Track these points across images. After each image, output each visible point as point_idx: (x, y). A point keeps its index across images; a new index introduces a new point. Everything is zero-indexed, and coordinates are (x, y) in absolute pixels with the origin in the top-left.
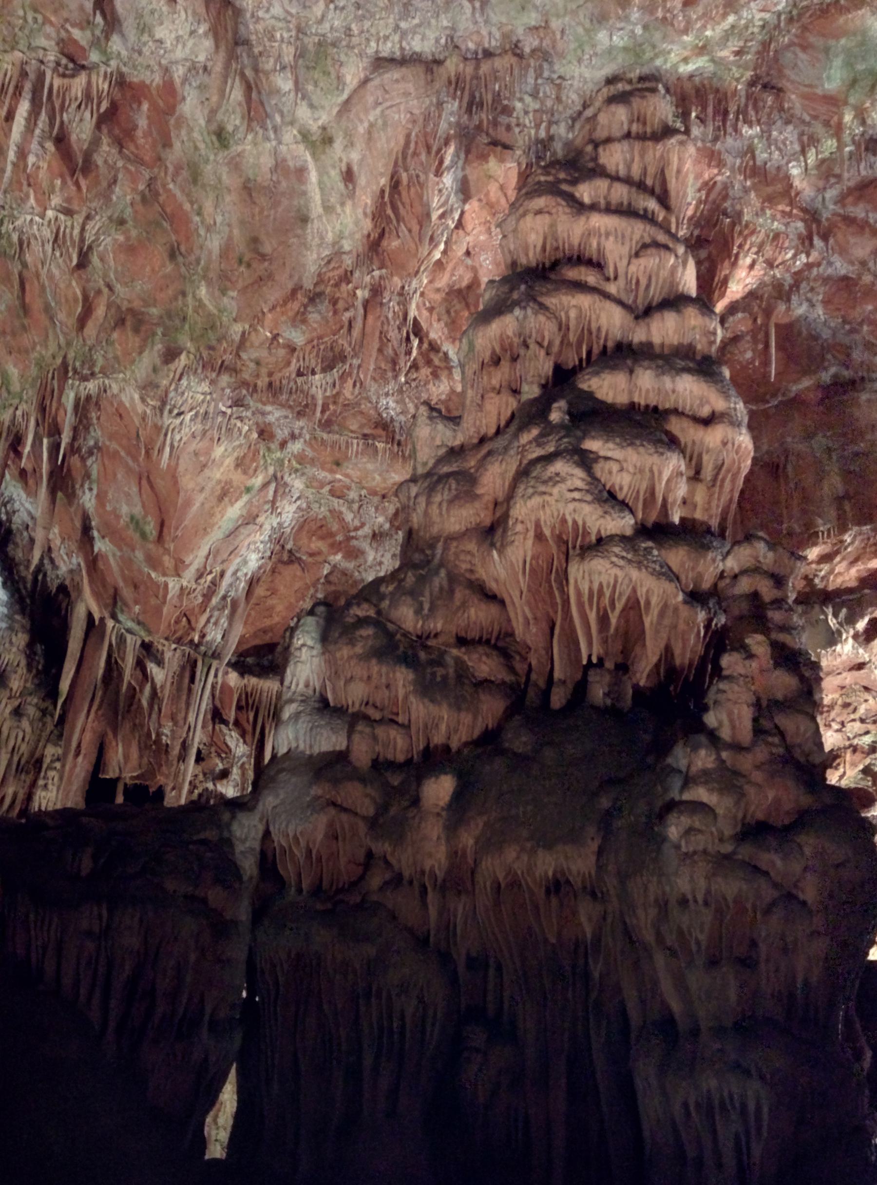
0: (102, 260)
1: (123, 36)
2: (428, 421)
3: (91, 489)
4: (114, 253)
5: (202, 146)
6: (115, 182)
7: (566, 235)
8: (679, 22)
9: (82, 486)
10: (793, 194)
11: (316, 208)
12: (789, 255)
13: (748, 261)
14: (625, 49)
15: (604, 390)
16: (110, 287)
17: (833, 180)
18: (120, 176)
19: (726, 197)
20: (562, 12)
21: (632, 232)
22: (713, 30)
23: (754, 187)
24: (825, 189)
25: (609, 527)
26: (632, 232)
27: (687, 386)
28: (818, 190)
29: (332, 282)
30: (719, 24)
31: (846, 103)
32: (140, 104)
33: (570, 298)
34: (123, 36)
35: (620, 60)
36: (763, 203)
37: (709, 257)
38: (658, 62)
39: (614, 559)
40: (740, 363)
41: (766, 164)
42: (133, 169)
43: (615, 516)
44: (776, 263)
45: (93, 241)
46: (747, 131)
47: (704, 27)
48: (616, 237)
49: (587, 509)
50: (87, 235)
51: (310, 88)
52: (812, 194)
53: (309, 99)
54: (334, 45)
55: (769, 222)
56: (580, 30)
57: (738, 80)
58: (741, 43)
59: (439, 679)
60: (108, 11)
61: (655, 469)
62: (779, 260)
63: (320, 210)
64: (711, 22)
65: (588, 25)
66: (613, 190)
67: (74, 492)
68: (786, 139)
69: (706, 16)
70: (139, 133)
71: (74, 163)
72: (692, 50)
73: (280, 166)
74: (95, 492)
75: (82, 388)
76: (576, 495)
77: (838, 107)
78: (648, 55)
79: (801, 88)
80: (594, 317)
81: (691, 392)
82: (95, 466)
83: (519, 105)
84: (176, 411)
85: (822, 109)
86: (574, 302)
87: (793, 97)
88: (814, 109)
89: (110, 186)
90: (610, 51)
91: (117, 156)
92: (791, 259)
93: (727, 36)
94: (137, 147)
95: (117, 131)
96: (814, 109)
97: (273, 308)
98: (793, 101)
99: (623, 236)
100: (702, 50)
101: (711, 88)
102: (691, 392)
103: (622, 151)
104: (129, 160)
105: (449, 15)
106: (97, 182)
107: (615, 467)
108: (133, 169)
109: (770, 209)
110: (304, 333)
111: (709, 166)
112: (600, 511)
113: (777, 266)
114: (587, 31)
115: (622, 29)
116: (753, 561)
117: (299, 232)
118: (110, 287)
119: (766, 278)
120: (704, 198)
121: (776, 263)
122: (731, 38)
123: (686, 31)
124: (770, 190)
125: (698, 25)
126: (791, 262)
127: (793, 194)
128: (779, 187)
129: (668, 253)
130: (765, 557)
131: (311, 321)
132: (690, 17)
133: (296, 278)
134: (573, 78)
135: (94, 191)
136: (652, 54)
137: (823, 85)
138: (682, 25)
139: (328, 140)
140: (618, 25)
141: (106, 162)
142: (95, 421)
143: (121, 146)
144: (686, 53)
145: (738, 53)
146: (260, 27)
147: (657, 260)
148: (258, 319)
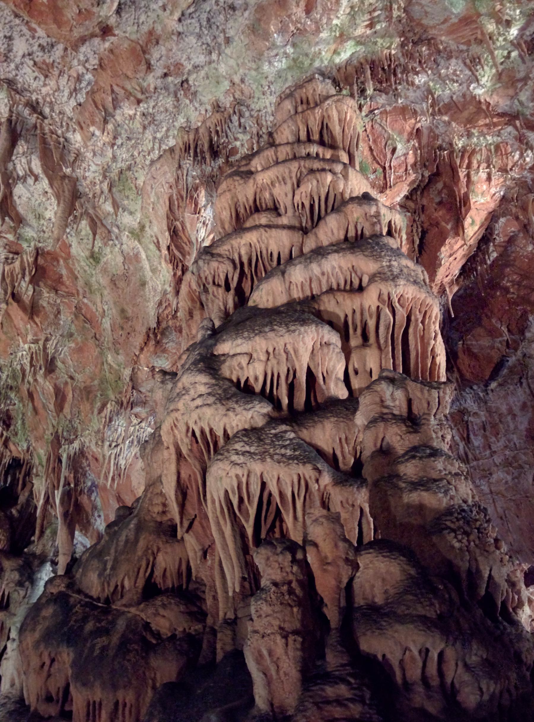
0: (63, 363)
1: (30, 226)
2: (161, 385)
3: (99, 516)
4: (70, 355)
5: (87, 268)
6: (59, 312)
7: (244, 200)
8: (310, 25)
9: (93, 515)
10: (484, 107)
11: (148, 274)
12: (517, 156)
13: (483, 175)
14: (289, 68)
15: (264, 299)
16: (72, 378)
17: (519, 85)
18: (61, 308)
19: (436, 137)
20: (237, 68)
21: (290, 172)
22: (338, 18)
23: (452, 119)
24: (517, 94)
25: (234, 425)
26: (290, 172)
27: (335, 264)
28: (512, 97)
29: (170, 317)
30: (338, 11)
31: (479, 15)
32: (58, 261)
33: (239, 240)
34: (30, 226)
35: (290, 78)
36: (465, 126)
37: (445, 186)
38: (317, 64)
39: (234, 458)
40: (527, 257)
41: (452, 97)
42: (66, 300)
43: (239, 409)
44: (509, 167)
45: (55, 353)
46: (420, 80)
47: (329, 19)
48: (280, 182)
49: (208, 412)
50: (49, 351)
51: (126, 202)
52: (508, 103)
53: (128, 210)
54: (129, 168)
55: (484, 140)
56: (254, 73)
57: (389, 48)
58: (367, 17)
59: (97, 652)
60: (13, 215)
61: (289, 348)
62: (510, 164)
63: (151, 274)
64: (331, 13)
65: (254, 66)
66: (279, 154)
67: (89, 522)
68: (455, 71)
69: (327, 11)
70: (65, 278)
71: (33, 310)
72: (334, 42)
73: (127, 259)
74: (103, 517)
75: (71, 448)
76: (199, 402)
77: (475, 21)
78: (307, 63)
79: (442, 27)
80: (263, 246)
81: (340, 268)
82: (98, 499)
83: (238, 143)
84: (114, 444)
85: (467, 32)
86: (243, 242)
87: (443, 38)
88: (463, 37)
89: (56, 316)
90: (279, 75)
91: (55, 297)
92: (520, 158)
93: (353, 15)
94: (67, 288)
95: (49, 282)
96: (463, 37)
97: (142, 349)
98: (445, 40)
99: (284, 179)
100: (342, 37)
101: (367, 61)
102: (340, 268)
103: (289, 127)
104: (63, 296)
105: (183, 114)
106: (46, 317)
107: (244, 361)
108: (66, 300)
109: (474, 127)
110: (167, 358)
111: (405, 119)
112: (222, 410)
113: (511, 169)
114: (257, 69)
115: (276, 55)
116: (378, 409)
117: (142, 293)
118: (72, 378)
119: (508, 183)
120: (417, 145)
121: (509, 167)
122: (357, 18)
123: (318, 31)
124: (466, 114)
125: (325, 21)
126: (521, 161)
127: (484, 107)
128: (472, 109)
129: (323, 174)
130: (394, 400)
131: (170, 349)
132: (315, 18)
133: (146, 324)
134: (265, 107)
135: (46, 323)
136: (309, 61)
137: (453, 13)
138: (313, 26)
139: (142, 228)
140: (273, 53)
141: (49, 303)
142: (88, 468)
143: (56, 291)
144: (333, 47)
145: (371, 26)
146: (88, 182)
147: (315, 183)
148: (136, 361)
